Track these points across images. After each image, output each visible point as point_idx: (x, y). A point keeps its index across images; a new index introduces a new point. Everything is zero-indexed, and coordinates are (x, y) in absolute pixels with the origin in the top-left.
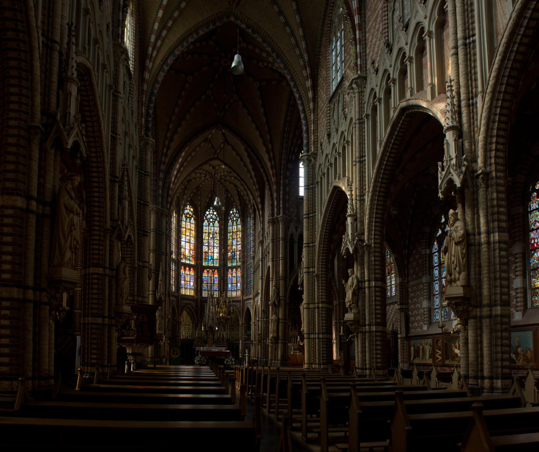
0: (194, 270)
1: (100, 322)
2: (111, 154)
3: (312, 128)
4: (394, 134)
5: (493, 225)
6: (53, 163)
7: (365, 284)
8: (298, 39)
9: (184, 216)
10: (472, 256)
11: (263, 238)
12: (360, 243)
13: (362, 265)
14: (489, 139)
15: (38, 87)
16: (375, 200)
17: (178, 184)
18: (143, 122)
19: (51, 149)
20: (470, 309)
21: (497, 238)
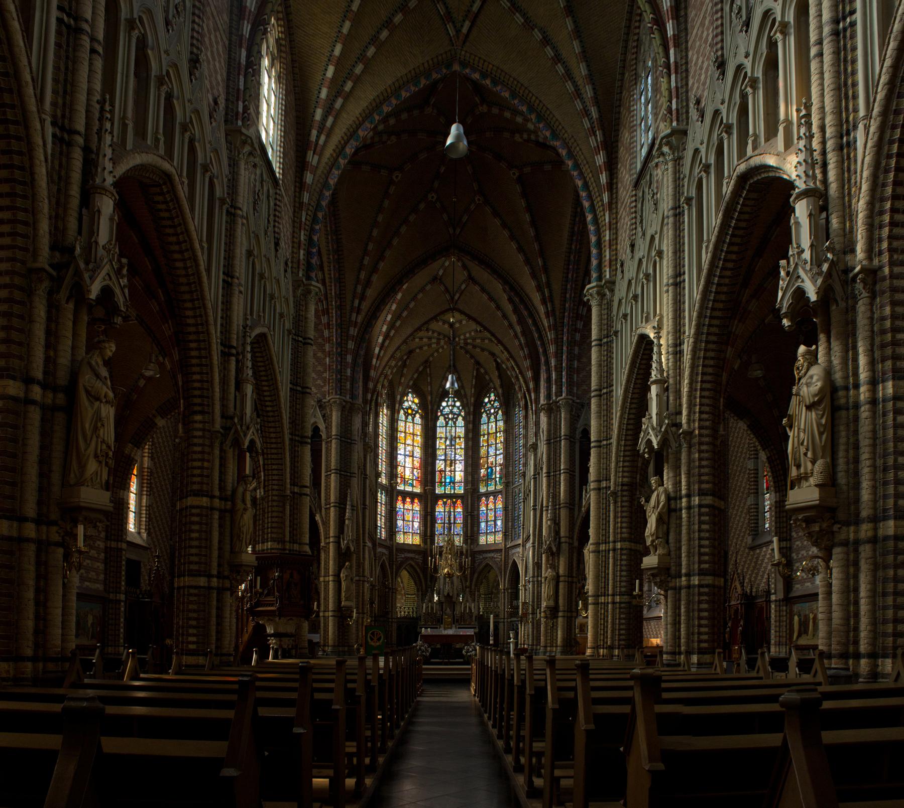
0: (420, 501)
1: (202, 584)
2: (222, 310)
3: (607, 238)
4: (730, 226)
5: (883, 367)
6: (71, 324)
7: (681, 503)
8: (579, 83)
9: (402, 412)
10: (842, 428)
11: (536, 440)
12: (674, 429)
13: (677, 469)
14: (877, 206)
15: (45, 207)
16: (700, 350)
17: (386, 359)
18: (302, 257)
19: (67, 303)
20: (836, 527)
21: (890, 391)
